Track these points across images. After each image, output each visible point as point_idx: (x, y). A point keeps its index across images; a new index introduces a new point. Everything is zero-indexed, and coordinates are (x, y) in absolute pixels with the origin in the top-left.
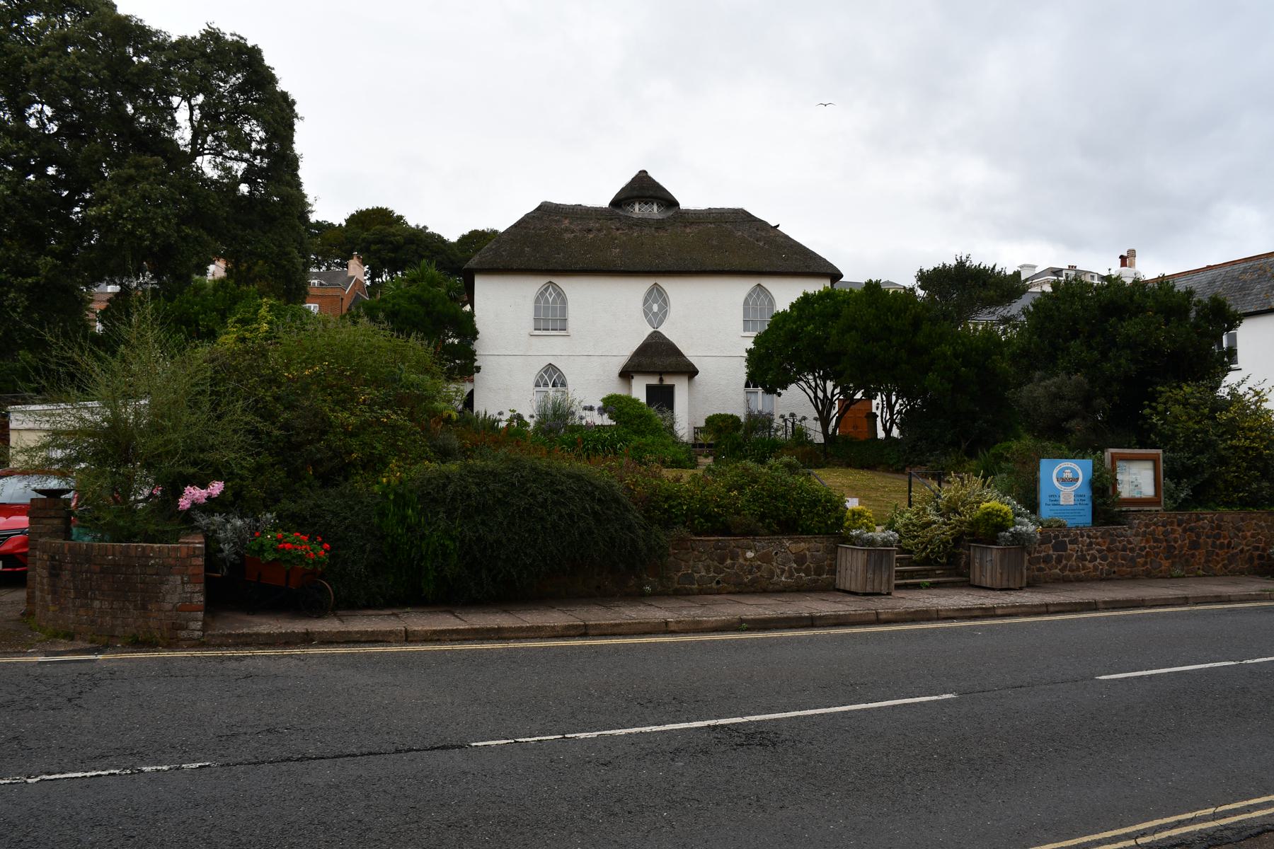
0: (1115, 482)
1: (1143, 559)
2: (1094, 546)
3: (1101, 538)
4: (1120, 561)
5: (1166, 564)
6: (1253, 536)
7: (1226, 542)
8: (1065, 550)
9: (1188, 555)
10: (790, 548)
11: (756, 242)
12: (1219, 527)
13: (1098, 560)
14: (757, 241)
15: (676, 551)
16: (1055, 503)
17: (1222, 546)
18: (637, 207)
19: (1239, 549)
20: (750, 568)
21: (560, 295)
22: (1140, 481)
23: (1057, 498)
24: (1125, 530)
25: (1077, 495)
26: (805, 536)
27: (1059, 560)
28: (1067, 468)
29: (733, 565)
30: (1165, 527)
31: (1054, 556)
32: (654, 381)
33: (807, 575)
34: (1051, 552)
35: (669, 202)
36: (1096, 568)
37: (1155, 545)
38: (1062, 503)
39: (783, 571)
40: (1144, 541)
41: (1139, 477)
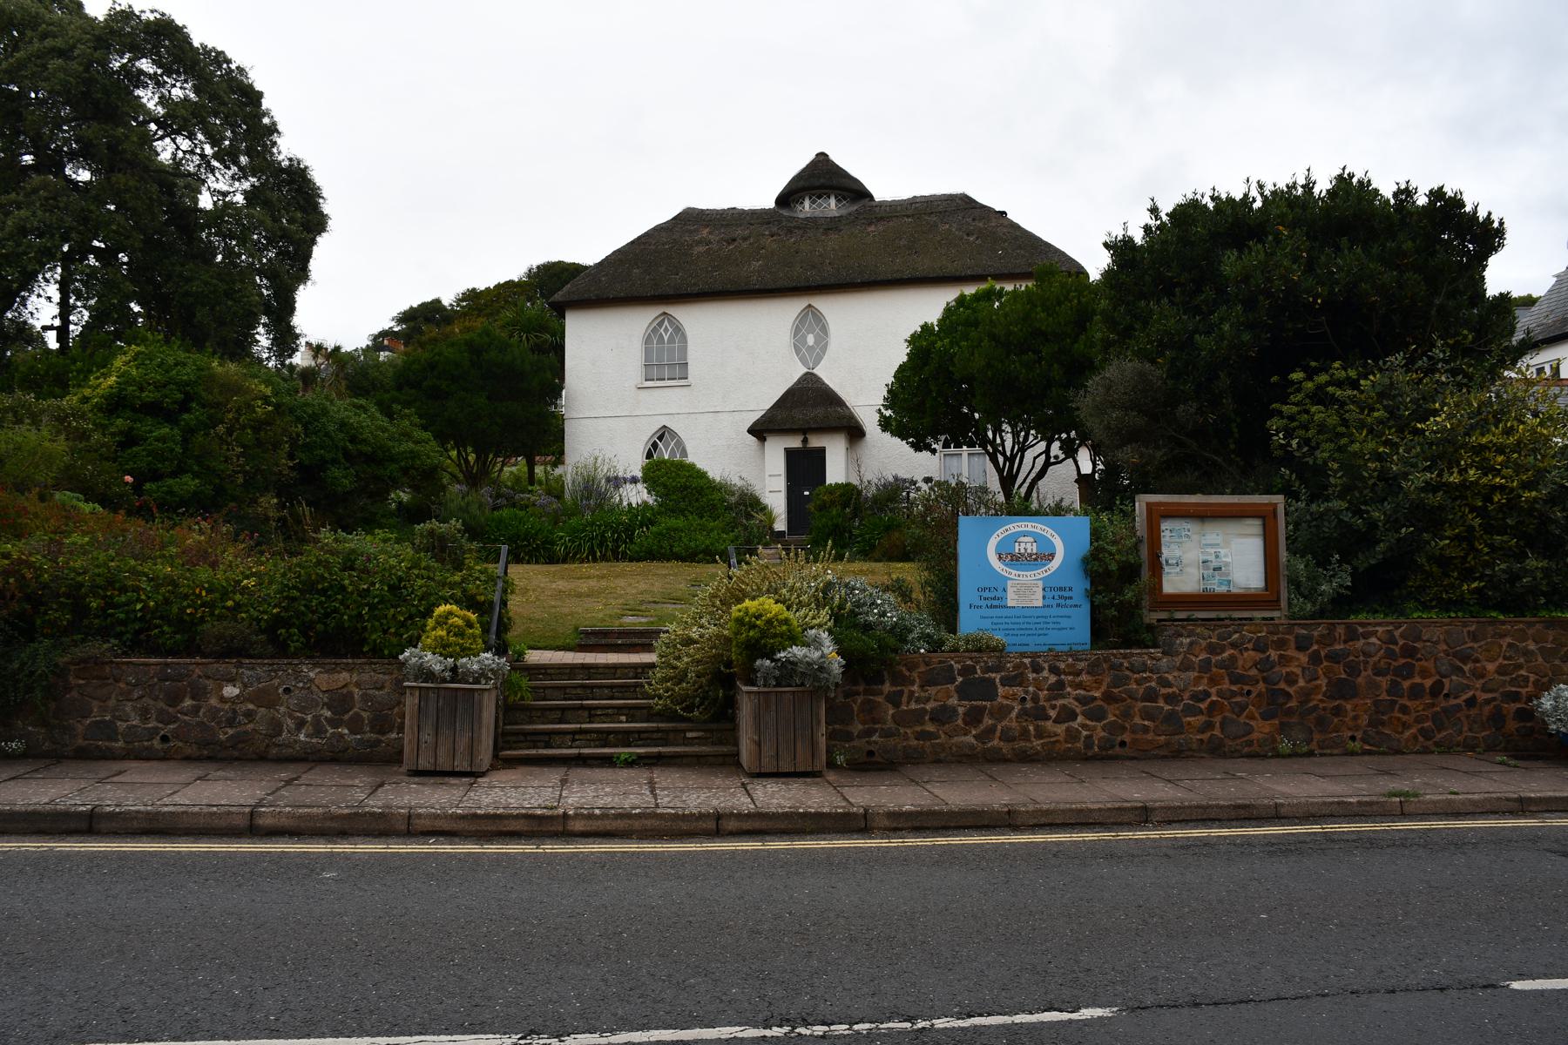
0: (1157, 567)
1: (1203, 718)
2: (1069, 689)
3: (1088, 673)
4: (1137, 720)
5: (1262, 728)
6: (1501, 671)
7: (1428, 683)
8: (992, 695)
9: (1324, 709)
10: (316, 682)
11: (966, 237)
12: (1409, 652)
13: (1080, 719)
14: (968, 235)
15: (81, 682)
16: (995, 603)
17: (1416, 692)
18: (807, 203)
19: (1465, 697)
20: (230, 715)
21: (678, 329)
22: (1229, 560)
23: (999, 594)
24: (1153, 659)
25: (1054, 590)
26: (350, 661)
27: (974, 717)
28: (1025, 534)
29: (195, 710)
30: (1263, 652)
31: (961, 710)
32: (795, 442)
33: (352, 732)
34: (953, 701)
35: (853, 191)
36: (1072, 735)
37: (1234, 688)
38: (1010, 604)
39: (301, 724)
40: (1206, 681)
41: (1223, 552)
